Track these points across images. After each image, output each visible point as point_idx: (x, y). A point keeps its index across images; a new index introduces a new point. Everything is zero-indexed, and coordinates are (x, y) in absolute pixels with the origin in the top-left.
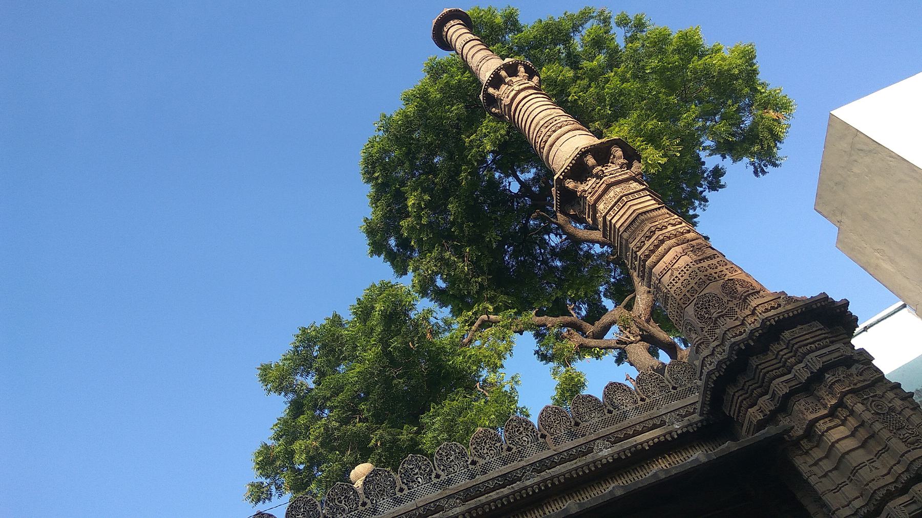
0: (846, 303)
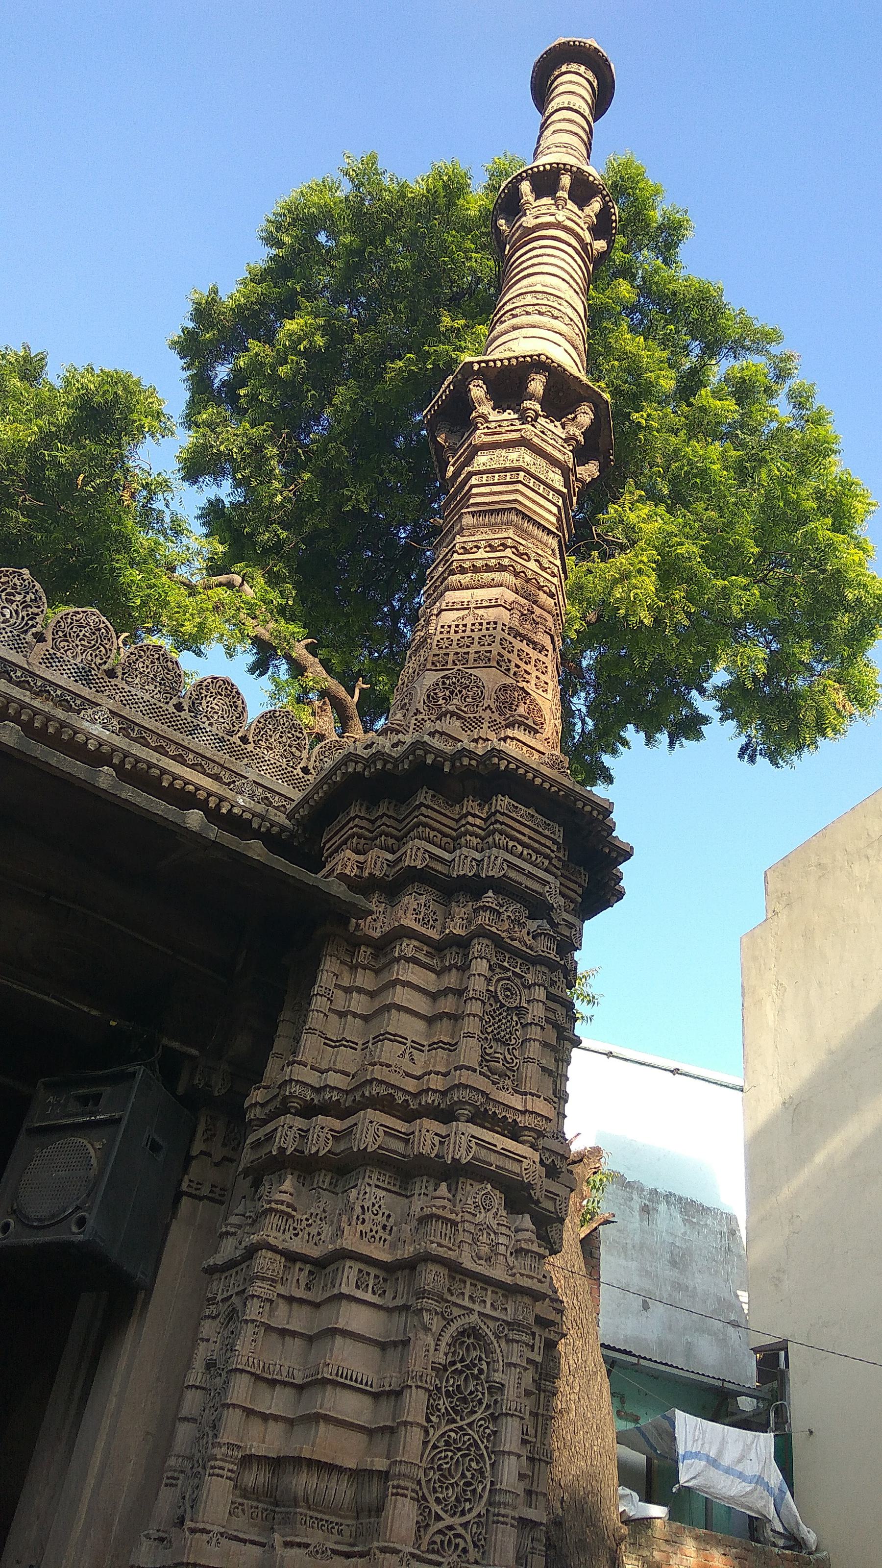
0: (626, 854)
